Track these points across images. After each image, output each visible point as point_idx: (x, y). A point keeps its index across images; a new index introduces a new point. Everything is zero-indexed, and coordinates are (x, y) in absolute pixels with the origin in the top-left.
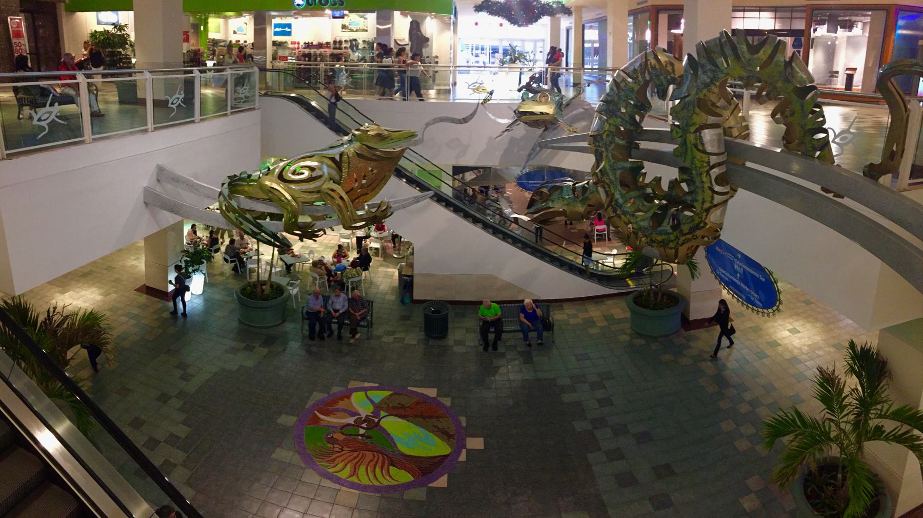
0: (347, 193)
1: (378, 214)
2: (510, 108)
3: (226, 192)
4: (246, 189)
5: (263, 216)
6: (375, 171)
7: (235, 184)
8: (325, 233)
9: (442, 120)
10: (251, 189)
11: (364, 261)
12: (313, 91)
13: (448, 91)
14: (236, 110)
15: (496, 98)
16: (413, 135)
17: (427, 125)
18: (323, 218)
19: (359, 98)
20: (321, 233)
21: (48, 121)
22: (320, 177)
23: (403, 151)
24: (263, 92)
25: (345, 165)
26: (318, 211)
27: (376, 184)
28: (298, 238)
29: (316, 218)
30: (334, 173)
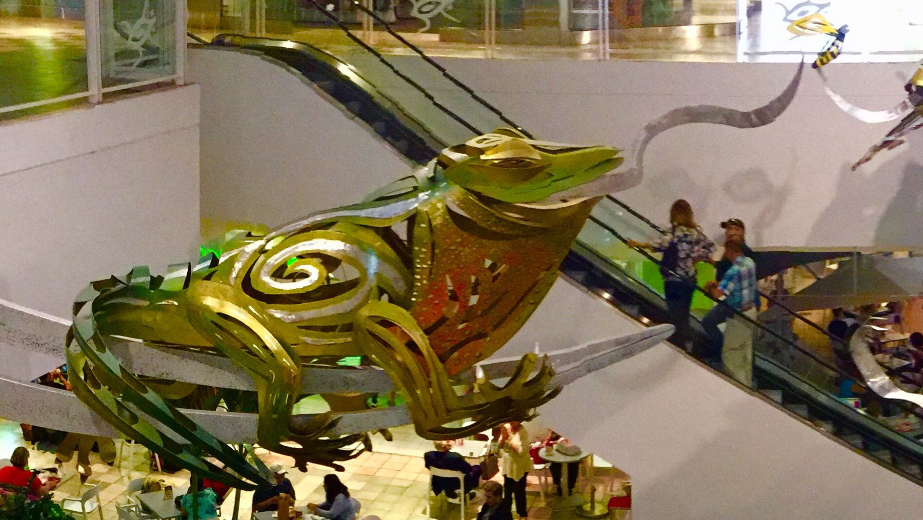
0: (427, 332)
1: (514, 393)
2: (900, 75)
3: (87, 329)
4: (146, 318)
5: (203, 397)
6: (502, 268)
7: (114, 304)
8: (369, 448)
9: (694, 115)
10: (159, 316)
11: (55, 482)
12: (342, 33)
13: (732, 30)
14: (117, 90)
15: (855, 51)
16: (609, 160)
17: (653, 130)
18: (361, 404)
19: (477, 54)
20: (358, 446)
21: (430, 15)
22: (352, 285)
23: (587, 206)
24: (207, 38)
25: (421, 252)
26: (347, 383)
27: (511, 303)
28: (291, 461)
29: (339, 404)
30: (392, 275)
